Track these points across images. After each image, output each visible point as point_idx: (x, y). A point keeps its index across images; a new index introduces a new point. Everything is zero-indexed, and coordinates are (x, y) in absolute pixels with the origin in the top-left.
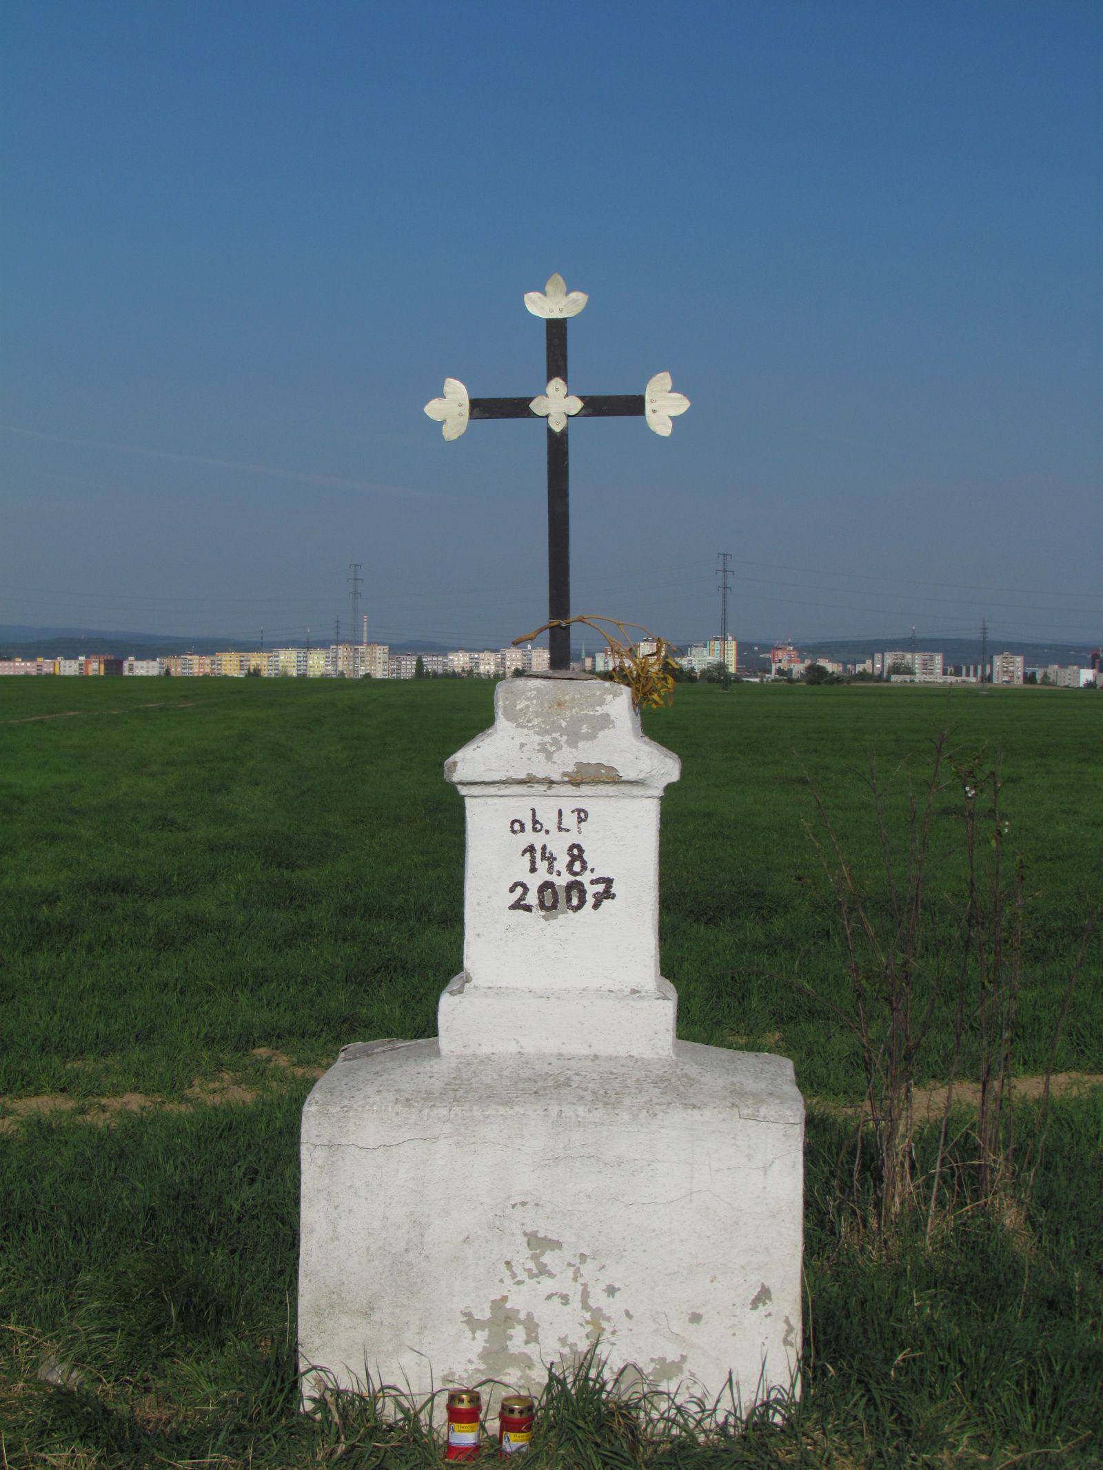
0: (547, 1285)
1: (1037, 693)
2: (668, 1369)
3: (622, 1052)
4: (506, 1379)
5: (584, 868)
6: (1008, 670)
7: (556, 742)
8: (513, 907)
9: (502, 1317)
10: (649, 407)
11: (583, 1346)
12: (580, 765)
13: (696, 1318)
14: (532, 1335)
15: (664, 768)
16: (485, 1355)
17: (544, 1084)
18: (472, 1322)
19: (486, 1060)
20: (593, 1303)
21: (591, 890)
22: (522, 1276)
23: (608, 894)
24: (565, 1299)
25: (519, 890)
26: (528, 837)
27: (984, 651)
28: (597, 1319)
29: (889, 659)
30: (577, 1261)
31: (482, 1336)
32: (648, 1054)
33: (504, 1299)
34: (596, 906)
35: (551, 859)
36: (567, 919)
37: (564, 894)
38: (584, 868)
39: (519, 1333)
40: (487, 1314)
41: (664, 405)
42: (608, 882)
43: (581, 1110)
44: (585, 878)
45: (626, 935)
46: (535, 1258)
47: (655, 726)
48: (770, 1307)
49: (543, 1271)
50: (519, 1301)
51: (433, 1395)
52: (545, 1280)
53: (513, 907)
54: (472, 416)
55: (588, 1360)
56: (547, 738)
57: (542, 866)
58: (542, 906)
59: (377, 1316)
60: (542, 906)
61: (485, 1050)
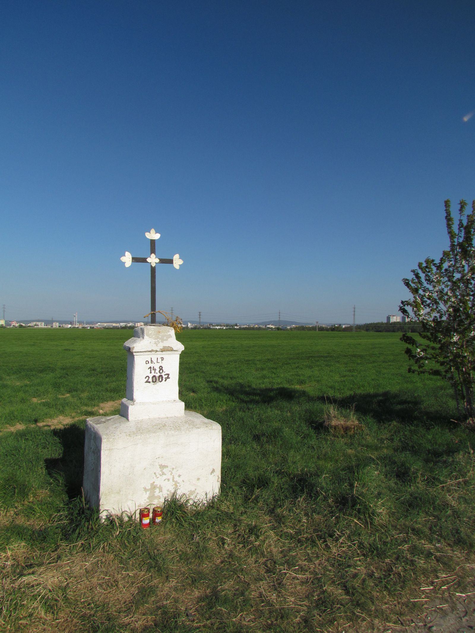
0: (164, 477)
1: (61, 329)
2: (192, 492)
3: (173, 416)
4: (154, 503)
5: (163, 371)
6: (56, 325)
7: (158, 341)
8: (146, 382)
9: (154, 487)
10: (174, 262)
11: (173, 491)
12: (164, 347)
13: (198, 479)
14: (161, 491)
15: (180, 347)
16: (149, 498)
17: (160, 426)
18: (145, 489)
19: (142, 421)
20: (175, 480)
21: (164, 377)
22: (158, 476)
23: (168, 378)
24: (169, 480)
25: (147, 378)
26: (150, 365)
27: (52, 322)
28: (176, 483)
29: (34, 323)
30: (171, 470)
31: (148, 493)
32: (179, 416)
33: (154, 482)
34: (165, 381)
35: (155, 370)
36: (159, 384)
37: (158, 378)
38: (163, 371)
39: (157, 490)
40: (150, 487)
41: (178, 262)
42: (168, 375)
43: (173, 432)
44: (163, 374)
45: (171, 387)
46: (161, 471)
47: (179, 337)
48: (215, 473)
49: (163, 474)
50: (157, 483)
51: (136, 511)
52: (164, 476)
53: (146, 382)
54: (132, 262)
55: (174, 494)
56: (156, 340)
57: (153, 371)
58: (153, 381)
59: (121, 493)
60: (153, 381)
61: (141, 419)
